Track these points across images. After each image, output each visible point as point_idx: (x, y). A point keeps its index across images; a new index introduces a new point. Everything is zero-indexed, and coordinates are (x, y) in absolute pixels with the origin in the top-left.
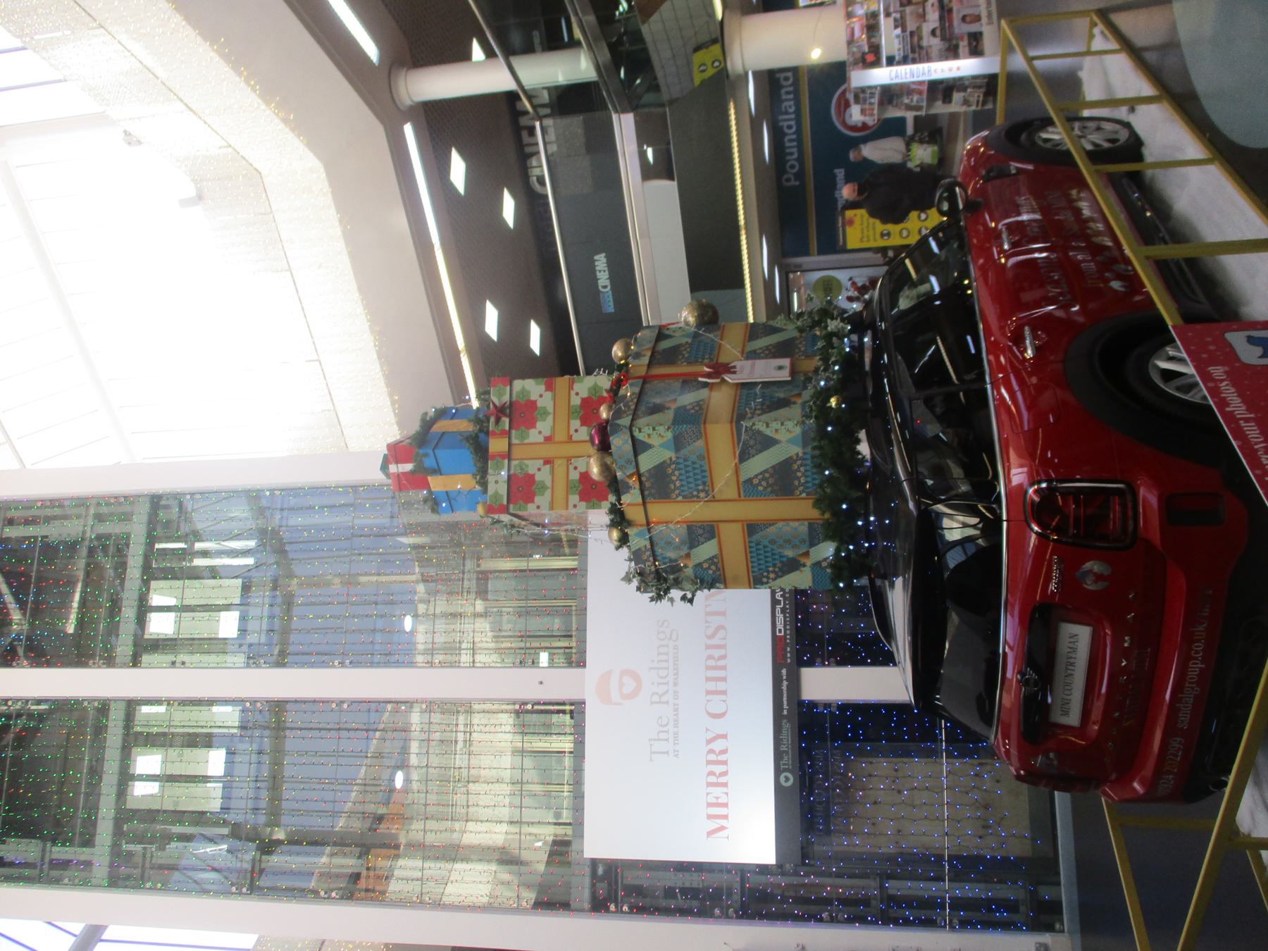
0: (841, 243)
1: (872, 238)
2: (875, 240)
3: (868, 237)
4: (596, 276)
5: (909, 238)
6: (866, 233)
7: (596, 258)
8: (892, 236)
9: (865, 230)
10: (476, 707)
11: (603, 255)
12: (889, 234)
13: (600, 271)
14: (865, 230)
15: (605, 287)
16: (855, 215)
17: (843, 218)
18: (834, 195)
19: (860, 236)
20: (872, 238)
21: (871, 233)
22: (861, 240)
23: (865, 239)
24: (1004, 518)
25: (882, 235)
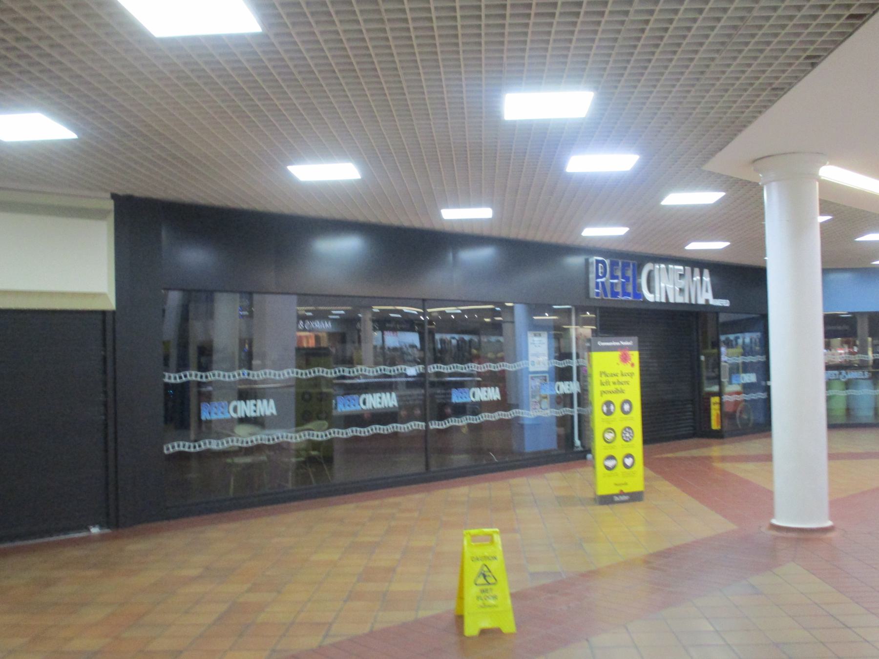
0: (600, 343)
1: (605, 388)
2: (603, 393)
3: (608, 383)
4: (250, 399)
5: (602, 441)
6: (611, 379)
7: (272, 402)
8: (605, 417)
9: (614, 379)
10: (616, 499)
11: (275, 412)
12: (609, 413)
13: (255, 405)
14: (614, 379)
15: (235, 410)
16: (633, 365)
17: (630, 348)
18: (729, 300)
19: (608, 371)
20: (605, 388)
21: (612, 387)
22: (603, 373)
23: (604, 379)
24: (421, 425)
25: (608, 403)
